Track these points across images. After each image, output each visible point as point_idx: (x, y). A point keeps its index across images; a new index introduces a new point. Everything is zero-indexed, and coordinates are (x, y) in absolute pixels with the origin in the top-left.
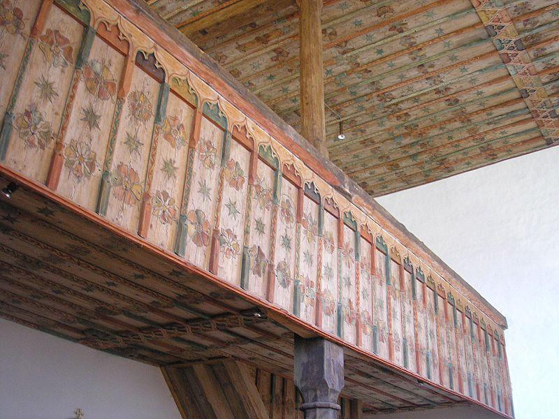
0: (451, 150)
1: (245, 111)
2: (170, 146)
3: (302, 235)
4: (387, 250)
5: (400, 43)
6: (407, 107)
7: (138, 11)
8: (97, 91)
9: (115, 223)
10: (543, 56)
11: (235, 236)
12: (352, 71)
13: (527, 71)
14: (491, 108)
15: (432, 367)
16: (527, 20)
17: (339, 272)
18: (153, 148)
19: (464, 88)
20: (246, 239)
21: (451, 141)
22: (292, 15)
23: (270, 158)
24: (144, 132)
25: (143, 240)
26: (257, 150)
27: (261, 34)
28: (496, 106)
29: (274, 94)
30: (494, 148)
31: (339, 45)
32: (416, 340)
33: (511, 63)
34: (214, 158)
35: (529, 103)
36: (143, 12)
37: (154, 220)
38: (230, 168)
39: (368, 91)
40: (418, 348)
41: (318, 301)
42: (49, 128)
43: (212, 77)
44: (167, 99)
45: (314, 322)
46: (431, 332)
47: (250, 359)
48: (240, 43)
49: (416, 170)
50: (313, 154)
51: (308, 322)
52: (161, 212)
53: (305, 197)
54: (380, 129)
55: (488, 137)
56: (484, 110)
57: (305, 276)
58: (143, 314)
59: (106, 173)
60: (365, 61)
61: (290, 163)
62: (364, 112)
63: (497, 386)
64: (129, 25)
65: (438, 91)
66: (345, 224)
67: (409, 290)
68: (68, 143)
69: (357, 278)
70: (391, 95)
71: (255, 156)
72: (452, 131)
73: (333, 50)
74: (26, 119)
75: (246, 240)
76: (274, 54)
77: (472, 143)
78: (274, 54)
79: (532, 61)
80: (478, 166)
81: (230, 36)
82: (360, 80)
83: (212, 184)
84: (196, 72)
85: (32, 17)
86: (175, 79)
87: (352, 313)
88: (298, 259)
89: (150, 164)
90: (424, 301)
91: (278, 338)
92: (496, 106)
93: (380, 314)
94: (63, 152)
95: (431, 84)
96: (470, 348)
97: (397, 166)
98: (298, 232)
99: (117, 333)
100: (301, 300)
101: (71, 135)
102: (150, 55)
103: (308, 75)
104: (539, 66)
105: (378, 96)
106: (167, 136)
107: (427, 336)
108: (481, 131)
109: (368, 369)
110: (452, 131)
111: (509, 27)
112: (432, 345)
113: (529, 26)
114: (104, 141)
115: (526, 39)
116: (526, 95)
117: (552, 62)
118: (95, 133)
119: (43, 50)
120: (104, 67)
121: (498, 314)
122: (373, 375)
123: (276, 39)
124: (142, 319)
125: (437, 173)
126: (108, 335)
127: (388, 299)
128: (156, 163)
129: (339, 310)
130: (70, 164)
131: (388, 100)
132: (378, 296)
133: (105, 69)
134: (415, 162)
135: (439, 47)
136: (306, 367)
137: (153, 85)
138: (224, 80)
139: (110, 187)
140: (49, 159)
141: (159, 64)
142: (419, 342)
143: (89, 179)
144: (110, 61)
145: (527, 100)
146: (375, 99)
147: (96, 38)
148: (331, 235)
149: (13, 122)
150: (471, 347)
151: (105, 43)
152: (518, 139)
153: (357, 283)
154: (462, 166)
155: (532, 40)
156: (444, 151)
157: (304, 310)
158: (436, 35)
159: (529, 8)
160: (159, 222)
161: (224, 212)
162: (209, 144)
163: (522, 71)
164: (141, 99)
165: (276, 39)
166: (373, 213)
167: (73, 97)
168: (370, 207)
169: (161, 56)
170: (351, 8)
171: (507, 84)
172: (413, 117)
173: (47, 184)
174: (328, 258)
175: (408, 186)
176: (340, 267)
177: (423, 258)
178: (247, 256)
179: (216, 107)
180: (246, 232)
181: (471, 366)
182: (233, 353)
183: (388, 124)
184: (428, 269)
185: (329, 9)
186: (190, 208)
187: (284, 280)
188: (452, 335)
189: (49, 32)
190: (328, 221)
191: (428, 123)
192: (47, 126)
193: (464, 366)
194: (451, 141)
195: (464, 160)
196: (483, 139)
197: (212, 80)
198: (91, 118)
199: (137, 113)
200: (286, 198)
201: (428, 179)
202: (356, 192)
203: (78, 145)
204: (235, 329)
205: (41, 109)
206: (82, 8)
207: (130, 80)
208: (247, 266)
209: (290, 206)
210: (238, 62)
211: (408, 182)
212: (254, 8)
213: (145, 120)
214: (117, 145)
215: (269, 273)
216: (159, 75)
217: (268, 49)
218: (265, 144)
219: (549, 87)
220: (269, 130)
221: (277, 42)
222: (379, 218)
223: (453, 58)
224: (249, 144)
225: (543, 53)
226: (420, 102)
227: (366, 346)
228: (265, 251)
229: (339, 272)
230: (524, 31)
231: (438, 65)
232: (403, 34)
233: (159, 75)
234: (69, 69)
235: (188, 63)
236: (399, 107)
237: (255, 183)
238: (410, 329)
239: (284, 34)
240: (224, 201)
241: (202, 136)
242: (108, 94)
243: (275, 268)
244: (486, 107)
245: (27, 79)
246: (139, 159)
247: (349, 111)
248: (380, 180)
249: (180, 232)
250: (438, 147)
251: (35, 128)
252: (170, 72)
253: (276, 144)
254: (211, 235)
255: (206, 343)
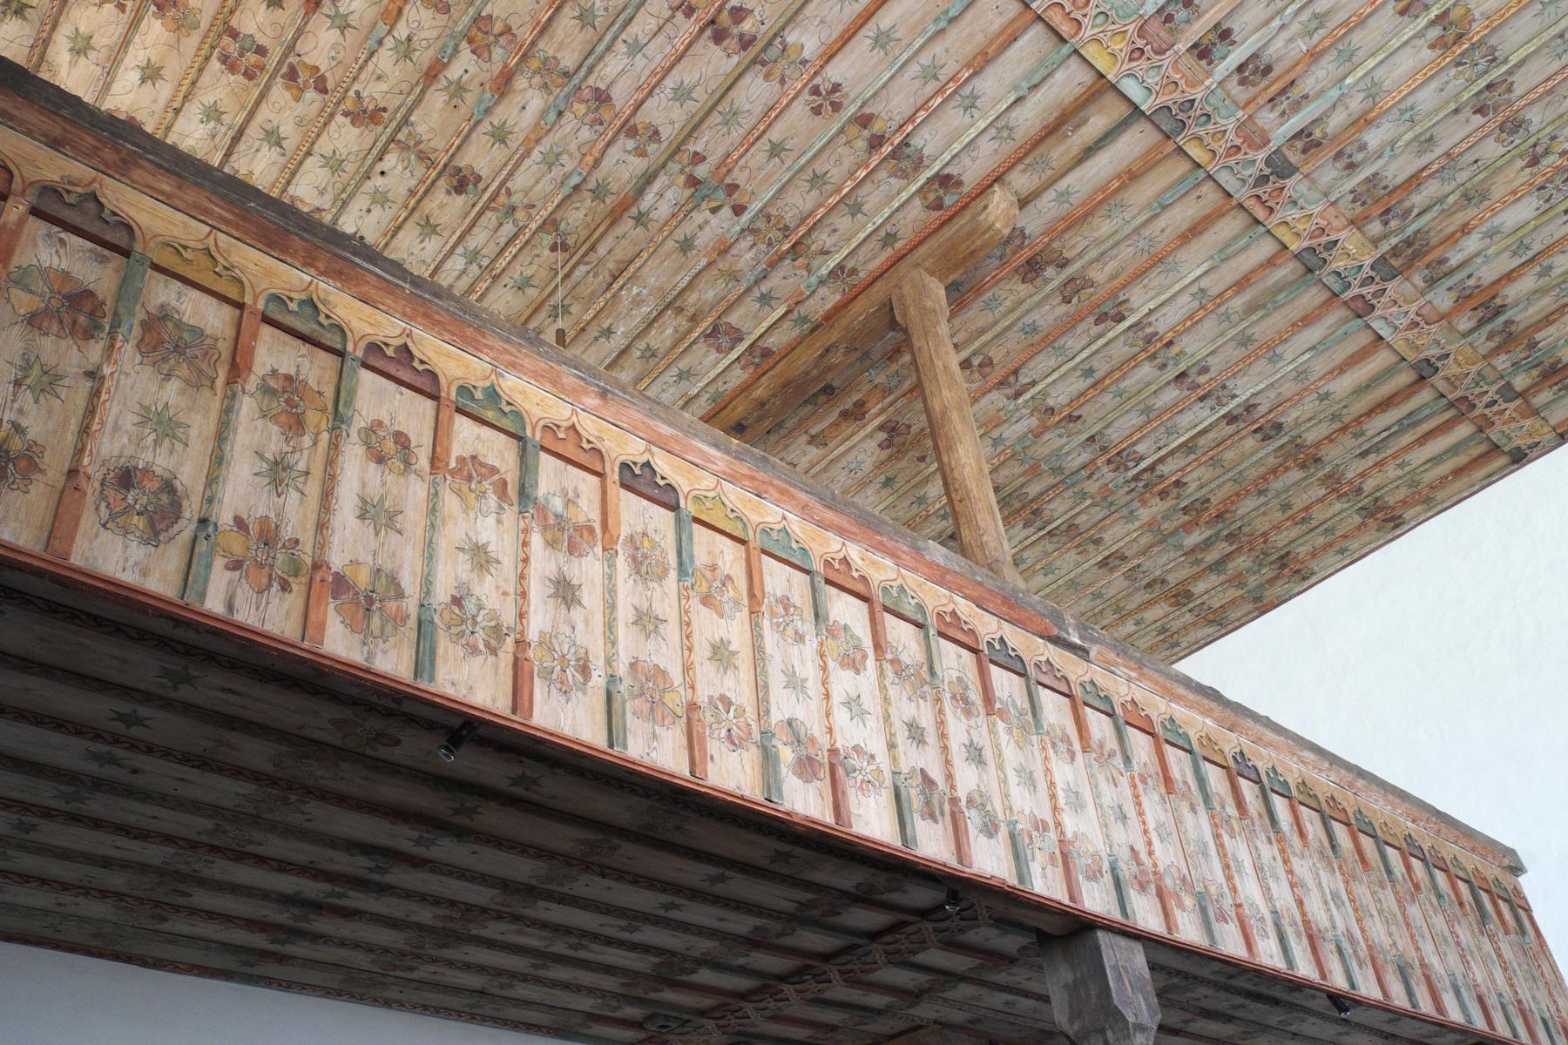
0: (1295, 532)
1: (841, 531)
2: (715, 616)
3: (1004, 738)
4: (1190, 743)
5: (1125, 344)
6: (1176, 467)
7: (603, 394)
8: (566, 544)
9: (647, 761)
10: (1446, 275)
11: (872, 757)
12: (1045, 428)
13: (1418, 319)
14: (1358, 420)
15: (1354, 966)
16: (1387, 211)
17: (1097, 796)
18: (685, 624)
19: (1287, 394)
20: (894, 757)
21: (1290, 512)
22: (898, 351)
23: (909, 608)
24: (663, 600)
25: (701, 782)
26: (879, 596)
27: (848, 404)
28: (1370, 413)
29: (901, 513)
30: (1391, 503)
31: (1002, 383)
32: (1303, 914)
33: (1377, 313)
34: (800, 623)
35: (1442, 386)
36: (613, 393)
37: (715, 746)
38: (834, 637)
39: (1085, 457)
40: (1310, 928)
41: (1065, 857)
42: (498, 618)
43: (764, 482)
44: (691, 538)
45: (1067, 897)
46: (1335, 896)
47: (970, 1022)
48: (813, 431)
49: (1233, 593)
50: (990, 584)
51: (1053, 897)
52: (724, 733)
53: (993, 668)
54: (1130, 527)
55: (1369, 485)
56: (1344, 429)
57: (1027, 812)
58: (742, 961)
59: (612, 679)
60: (1063, 399)
61: (949, 609)
62: (1089, 502)
63: (1534, 998)
64: (593, 421)
65: (1231, 418)
66: (1086, 704)
67: (1260, 816)
68: (536, 639)
69: (1139, 804)
70: (1135, 452)
71: (878, 609)
72: (1287, 491)
73: (994, 395)
74: (457, 610)
75: (894, 759)
76: (882, 436)
77: (1338, 506)
78: (882, 436)
79: (1423, 294)
80: (1366, 550)
81: (789, 424)
82: (1064, 440)
83: (809, 670)
84: (733, 479)
85: (427, 440)
86: (696, 498)
87: (1143, 872)
88: (1005, 781)
89: (686, 653)
90: (1302, 834)
91: (1012, 961)
92: (1370, 413)
93: (1205, 868)
94: (530, 654)
95: (1212, 409)
96: (1439, 922)
97: (1189, 595)
98: (992, 731)
99: (702, 1013)
100: (1030, 857)
101: (537, 624)
102: (643, 465)
103: (950, 449)
104: (1443, 299)
105: (1109, 462)
106: (706, 600)
107: (1326, 903)
108: (1350, 475)
109: (1221, 1002)
110: (1287, 491)
111: (1350, 240)
112: (1344, 920)
113: (1393, 224)
114: (598, 620)
115: (1395, 252)
116: (1429, 371)
117: (1471, 282)
118: (577, 614)
119: (458, 493)
120: (568, 502)
121: (1493, 844)
122: (1238, 1013)
123: (879, 406)
124: (742, 970)
125: (1278, 589)
126: (688, 1021)
127: (1217, 837)
128: (696, 648)
129: (1113, 869)
130: (547, 674)
131: (1131, 464)
132: (1192, 834)
133: (570, 505)
134: (1223, 578)
135: (1209, 327)
136: (1074, 989)
137: (661, 518)
138: (786, 481)
139: (624, 702)
140: (510, 672)
141: (663, 478)
142: (1310, 917)
143: (585, 693)
144: (576, 490)
145: (1438, 381)
146: (1105, 469)
147: (543, 456)
148: (1063, 730)
149: (436, 619)
150: (1441, 918)
151: (559, 462)
152: (1444, 468)
153: (1141, 813)
154: (1330, 559)
155: (1410, 251)
156: (1281, 539)
157: (1038, 875)
158: (1196, 304)
159: (1384, 183)
160: (724, 749)
161: (841, 716)
162: (785, 602)
163: (1405, 322)
164: (646, 543)
165: (879, 406)
166: (1142, 675)
167: (526, 561)
168: (1132, 664)
169: (663, 464)
170: (1008, 303)
171: (1382, 359)
172: (1193, 486)
173: (514, 711)
174: (1064, 773)
175: (1223, 631)
176: (1096, 786)
177: (1276, 748)
178: (902, 790)
179: (782, 534)
180: (891, 746)
181: (1453, 959)
182: (934, 1015)
183: (1145, 514)
184: (1293, 769)
185: (966, 316)
186: (776, 716)
187: (986, 825)
188: (1389, 900)
189: (461, 460)
190: (1050, 704)
191: (1229, 489)
192: (494, 615)
193: (1434, 960)
194: (1290, 512)
195: (1330, 545)
196: (1359, 490)
197: (765, 487)
198: (565, 592)
199: (644, 569)
200: (955, 674)
201: (1262, 606)
202: (1094, 641)
203: (554, 640)
204: (921, 958)
205: (476, 590)
206: (507, 409)
207: (617, 514)
208: (905, 805)
209: (967, 688)
210: (817, 468)
211: (1221, 623)
212: (822, 356)
213: (662, 576)
214: (621, 630)
215: (953, 814)
216: (666, 497)
217: (869, 428)
218: (893, 584)
219: (1480, 338)
220: (893, 555)
221: (883, 411)
222: (1157, 683)
223: (1244, 341)
224: (860, 588)
225: (1445, 268)
226: (1199, 452)
227: (1189, 931)
228: (936, 774)
229: (1097, 796)
230: (1385, 236)
231: (1215, 363)
232: (1126, 324)
233: (666, 497)
234: (510, 514)
235: (715, 467)
236: (1158, 473)
237: (889, 656)
238: (1283, 895)
239: (890, 393)
240: (837, 697)
241: (768, 589)
242: (585, 545)
243: (963, 803)
244: (1346, 420)
245: (443, 546)
246: (665, 647)
247: (1058, 509)
248: (1160, 633)
249: (768, 758)
250: (1265, 534)
251: (475, 623)
252: (686, 489)
253: (912, 579)
254: (826, 760)
255: (877, 1000)
